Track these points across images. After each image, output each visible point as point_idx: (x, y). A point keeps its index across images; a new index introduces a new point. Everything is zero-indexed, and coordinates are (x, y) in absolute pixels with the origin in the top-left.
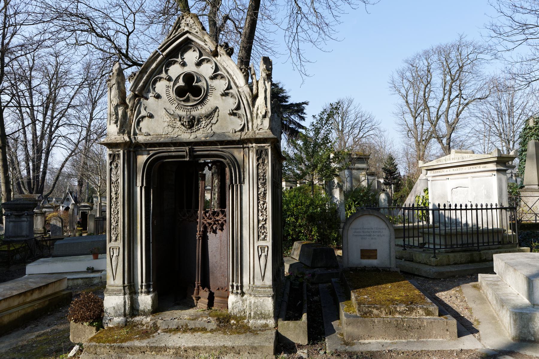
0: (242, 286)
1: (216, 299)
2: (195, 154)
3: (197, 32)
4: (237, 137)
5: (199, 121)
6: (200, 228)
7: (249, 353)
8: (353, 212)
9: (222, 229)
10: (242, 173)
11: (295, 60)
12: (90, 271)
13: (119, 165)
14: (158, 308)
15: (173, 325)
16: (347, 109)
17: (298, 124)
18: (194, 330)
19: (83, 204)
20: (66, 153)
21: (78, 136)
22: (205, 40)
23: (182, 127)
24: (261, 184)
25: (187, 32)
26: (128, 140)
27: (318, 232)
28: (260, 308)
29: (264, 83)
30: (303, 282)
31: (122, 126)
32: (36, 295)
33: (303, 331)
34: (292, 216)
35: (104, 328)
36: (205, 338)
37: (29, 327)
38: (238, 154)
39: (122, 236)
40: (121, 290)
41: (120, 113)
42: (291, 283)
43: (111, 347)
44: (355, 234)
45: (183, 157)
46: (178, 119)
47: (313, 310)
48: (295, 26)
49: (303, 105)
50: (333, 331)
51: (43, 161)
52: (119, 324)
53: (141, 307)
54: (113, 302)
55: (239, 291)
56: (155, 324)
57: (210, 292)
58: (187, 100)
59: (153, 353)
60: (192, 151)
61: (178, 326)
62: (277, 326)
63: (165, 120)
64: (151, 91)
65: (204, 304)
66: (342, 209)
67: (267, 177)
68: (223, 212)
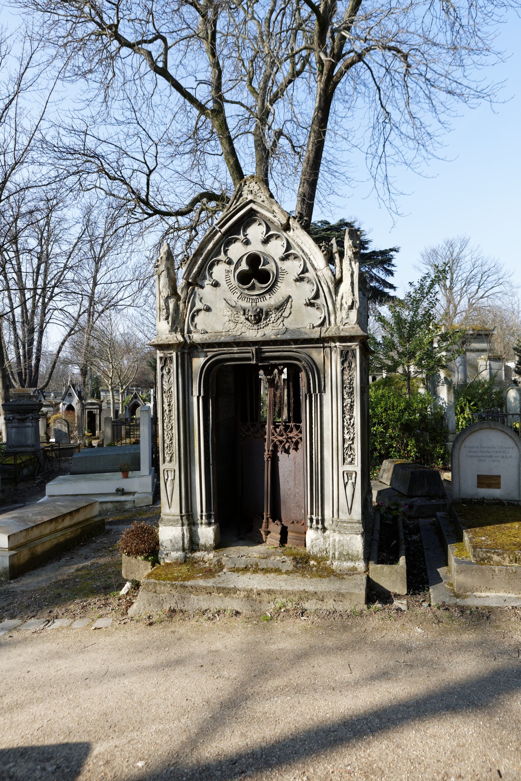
0: (323, 520)
1: (290, 535)
2: (263, 355)
3: (263, 201)
4: (315, 334)
5: (267, 314)
6: (268, 447)
7: (334, 600)
8: (466, 416)
9: (296, 449)
10: (322, 380)
11: (381, 193)
12: (120, 493)
13: (172, 371)
14: (220, 543)
15: (240, 564)
16: (458, 254)
17: (384, 281)
18: (266, 571)
19: (89, 401)
20: (65, 331)
21: (77, 308)
22: (274, 211)
23: (247, 322)
24: (347, 393)
25: (251, 201)
26: (182, 340)
27: (416, 447)
28: (346, 548)
29: (351, 264)
30: (398, 516)
31: (173, 323)
32: (67, 522)
33: (402, 578)
34: (379, 424)
35: (160, 564)
36: (281, 580)
37: (63, 560)
38: (317, 355)
39: (177, 456)
40: (178, 520)
41: (171, 306)
42: (382, 516)
43: (172, 585)
44: (471, 454)
45: (249, 359)
46: (242, 313)
47: (411, 552)
48: (382, 140)
49: (391, 253)
50: (438, 580)
51: (35, 343)
52: (177, 559)
53: (202, 541)
54: (170, 534)
55: (320, 526)
56: (219, 561)
57: (283, 525)
58: (253, 288)
59: (221, 594)
60: (259, 352)
61: (247, 565)
62: (367, 570)
63: (225, 314)
64: (208, 277)
65: (276, 539)
66: (451, 413)
67: (354, 385)
68: (298, 428)
